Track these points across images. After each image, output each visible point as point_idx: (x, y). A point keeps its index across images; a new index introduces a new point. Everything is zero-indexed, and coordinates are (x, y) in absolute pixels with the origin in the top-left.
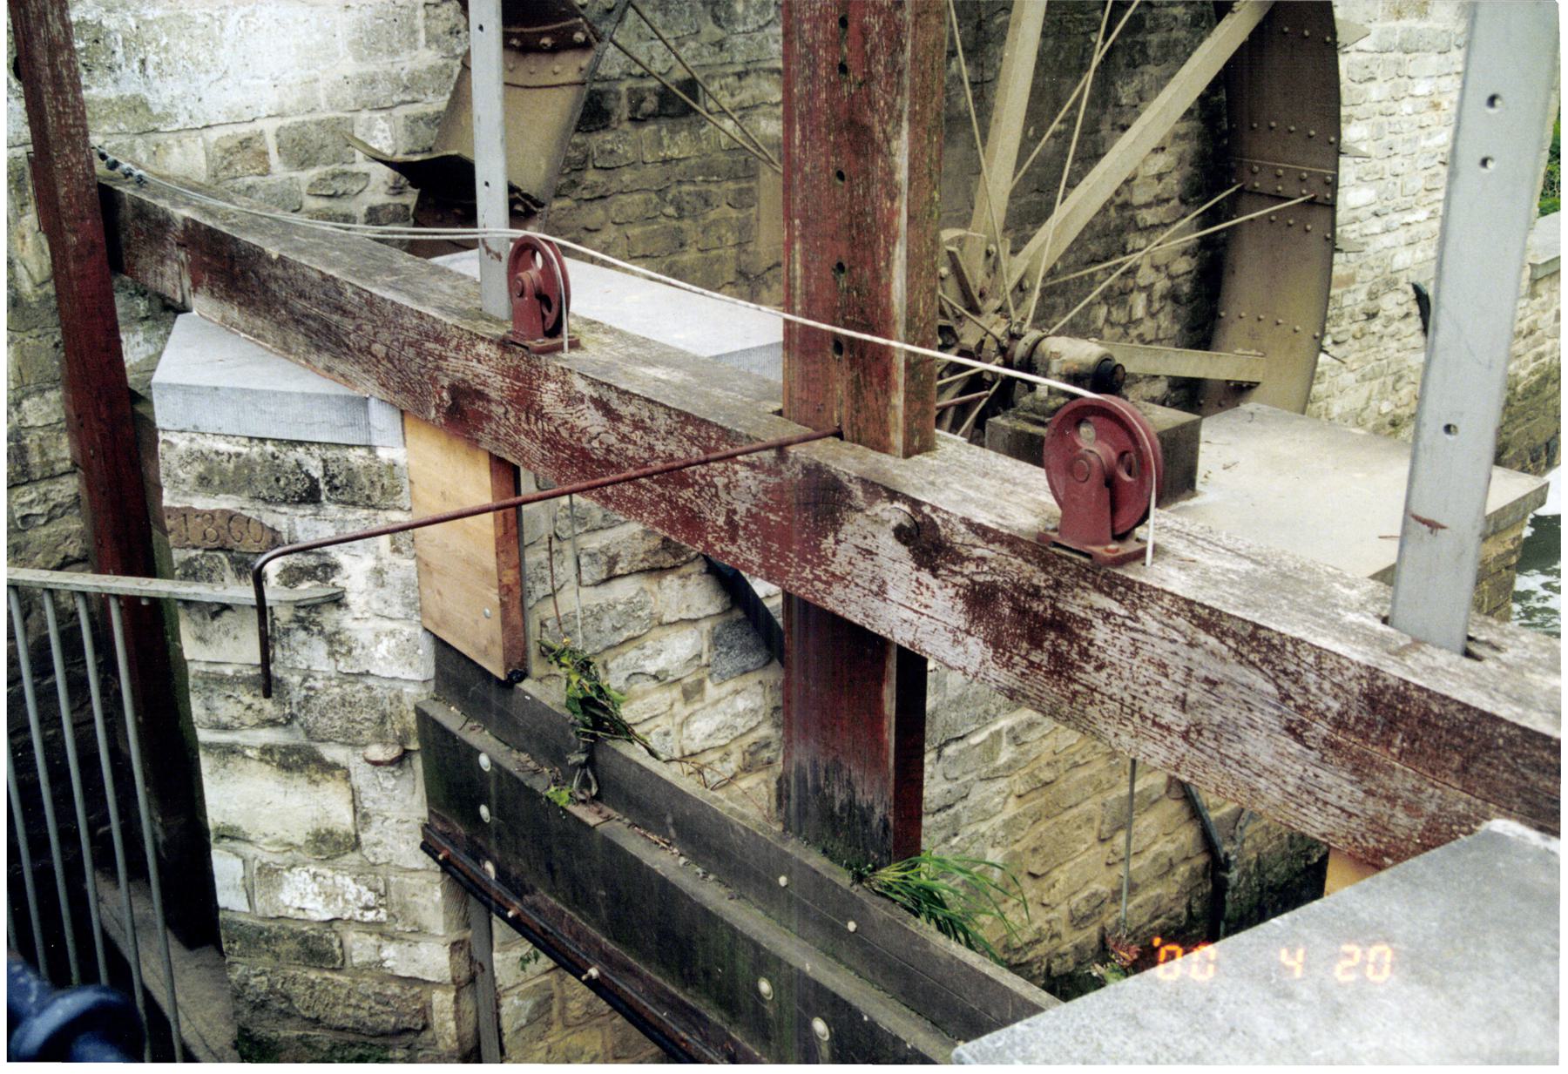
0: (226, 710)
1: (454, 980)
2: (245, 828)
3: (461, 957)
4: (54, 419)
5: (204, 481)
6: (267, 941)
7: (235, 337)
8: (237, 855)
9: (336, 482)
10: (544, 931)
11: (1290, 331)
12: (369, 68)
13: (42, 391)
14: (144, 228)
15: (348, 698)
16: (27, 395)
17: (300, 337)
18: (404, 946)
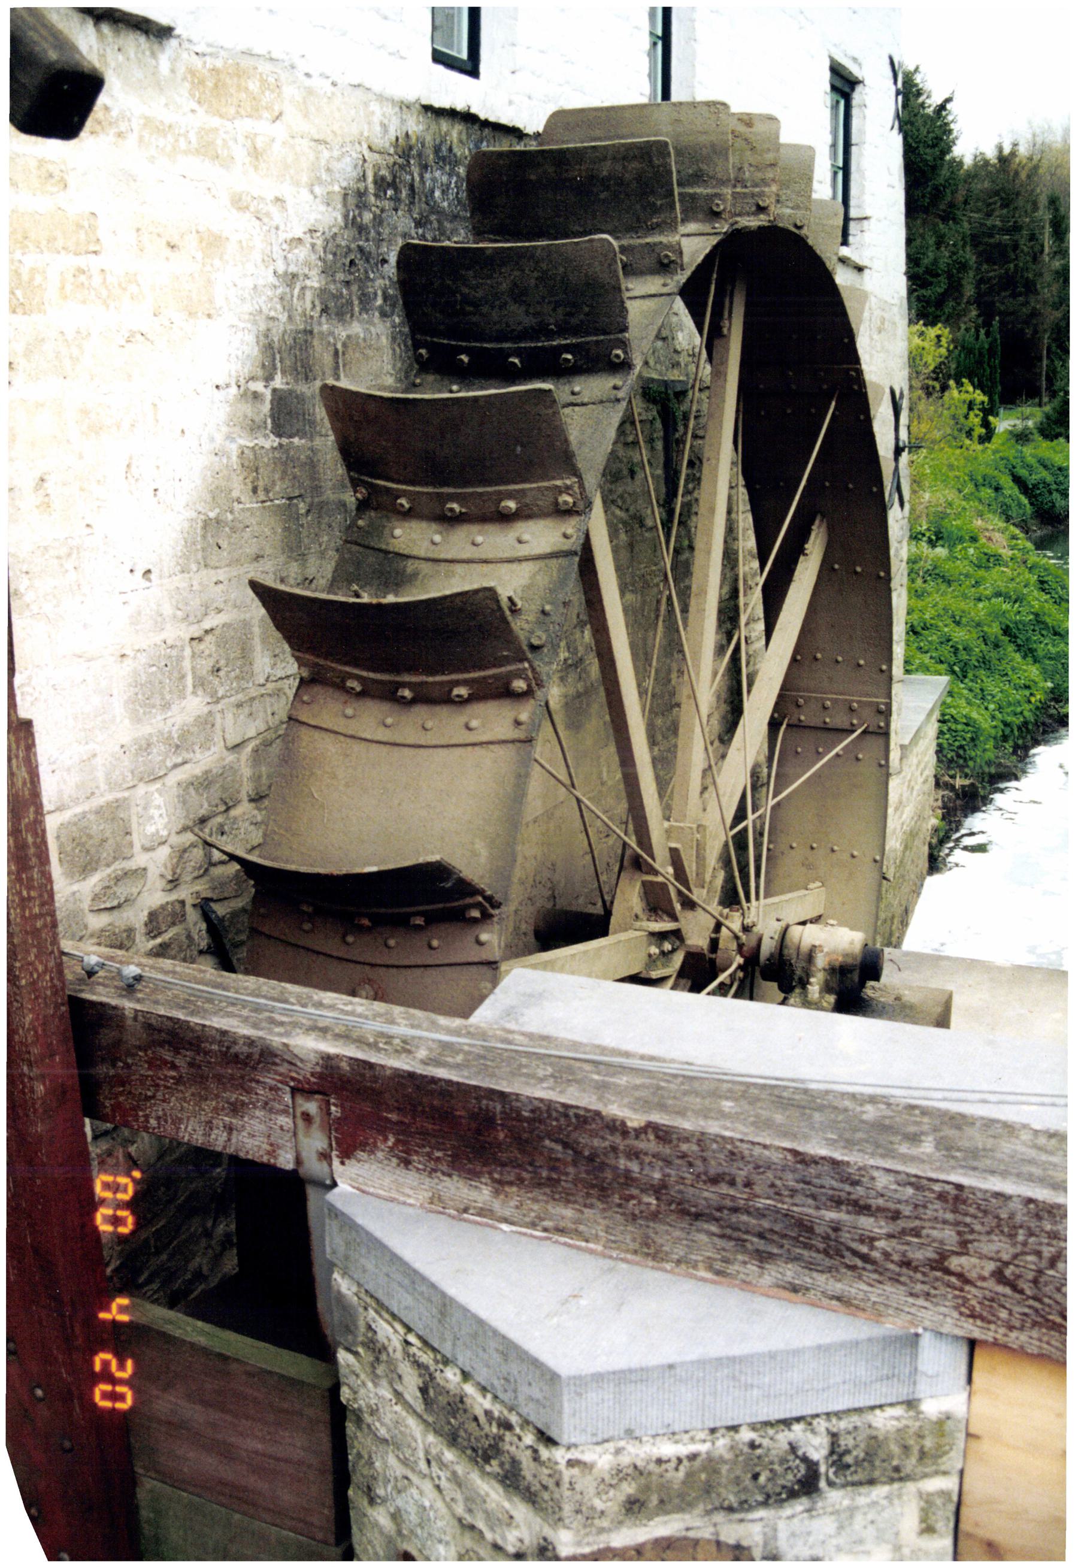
5: (634, 1507)
9: (849, 1459)
11: (846, 856)
12: (146, 730)
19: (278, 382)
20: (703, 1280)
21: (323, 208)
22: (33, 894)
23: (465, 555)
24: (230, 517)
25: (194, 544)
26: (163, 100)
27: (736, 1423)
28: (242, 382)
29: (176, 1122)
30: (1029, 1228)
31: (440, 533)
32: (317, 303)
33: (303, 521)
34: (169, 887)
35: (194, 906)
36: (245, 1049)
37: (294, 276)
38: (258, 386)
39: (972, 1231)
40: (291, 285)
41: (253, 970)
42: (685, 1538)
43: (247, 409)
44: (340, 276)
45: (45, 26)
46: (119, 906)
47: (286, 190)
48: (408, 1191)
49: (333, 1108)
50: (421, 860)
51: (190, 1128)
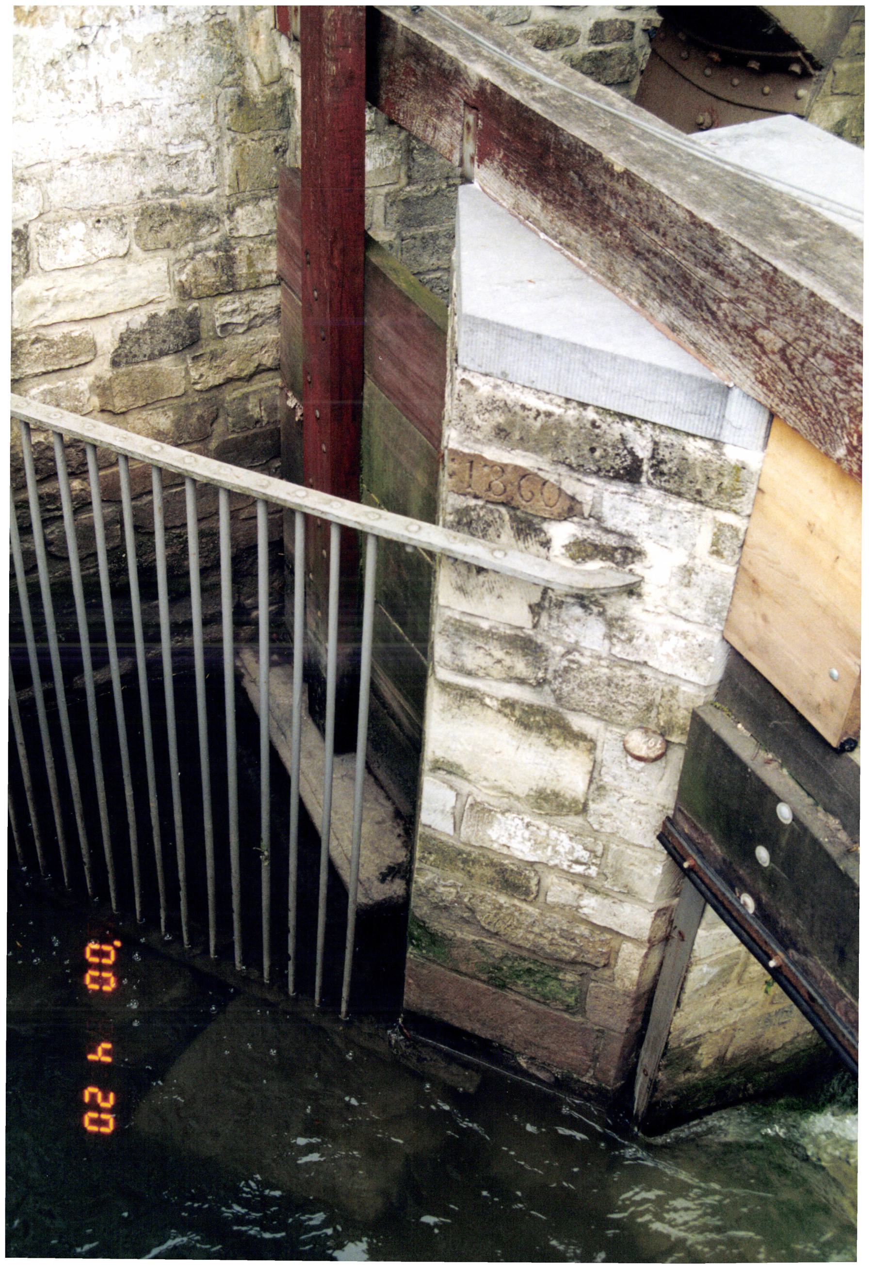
0: (472, 658)
1: (649, 941)
2: (465, 768)
3: (662, 922)
4: (265, 230)
5: (501, 433)
6: (465, 861)
7: (533, 237)
8: (451, 787)
9: (664, 468)
10: (813, 999)
13: (257, 199)
14: (419, 71)
15: (615, 680)
16: (241, 203)
17: (637, 273)
18: (609, 901)
20: (631, 306)
27: (586, 401)
30: (807, 318)
35: (645, 31)
39: (775, 310)
42: (536, 475)
48: (505, 197)
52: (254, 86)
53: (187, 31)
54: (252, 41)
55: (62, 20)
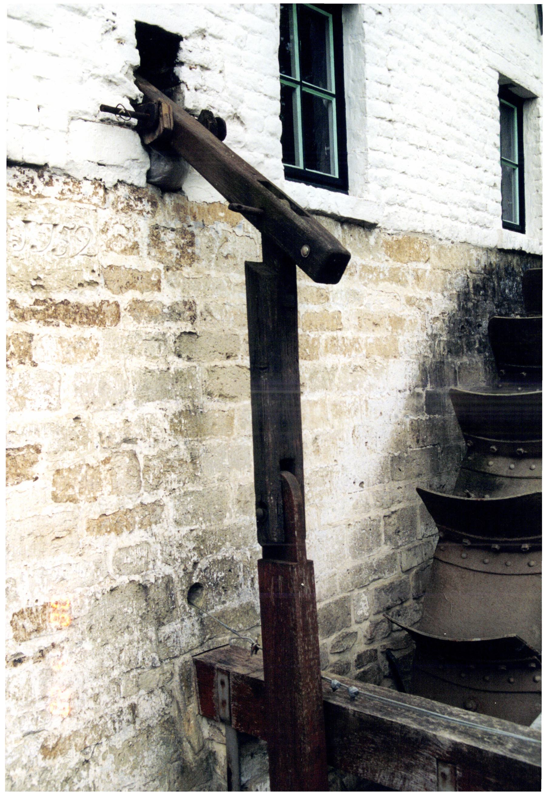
12: (359, 562)
19: (429, 388)
21: (448, 302)
22: (310, 648)
23: (527, 475)
24: (406, 455)
25: (386, 468)
26: (371, 257)
28: (412, 388)
29: (374, 772)
31: (514, 463)
32: (446, 348)
33: (440, 456)
34: (368, 642)
35: (382, 652)
36: (414, 736)
37: (436, 335)
38: (419, 390)
40: (434, 340)
41: (415, 692)
43: (414, 401)
44: (457, 334)
45: (326, 234)
46: (343, 651)
47: (432, 294)
49: (458, 772)
50: (505, 636)
51: (381, 776)
52: (190, 756)
53: (148, 731)
54: (186, 727)
55: (74, 747)
